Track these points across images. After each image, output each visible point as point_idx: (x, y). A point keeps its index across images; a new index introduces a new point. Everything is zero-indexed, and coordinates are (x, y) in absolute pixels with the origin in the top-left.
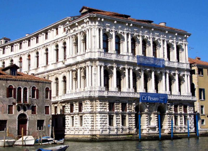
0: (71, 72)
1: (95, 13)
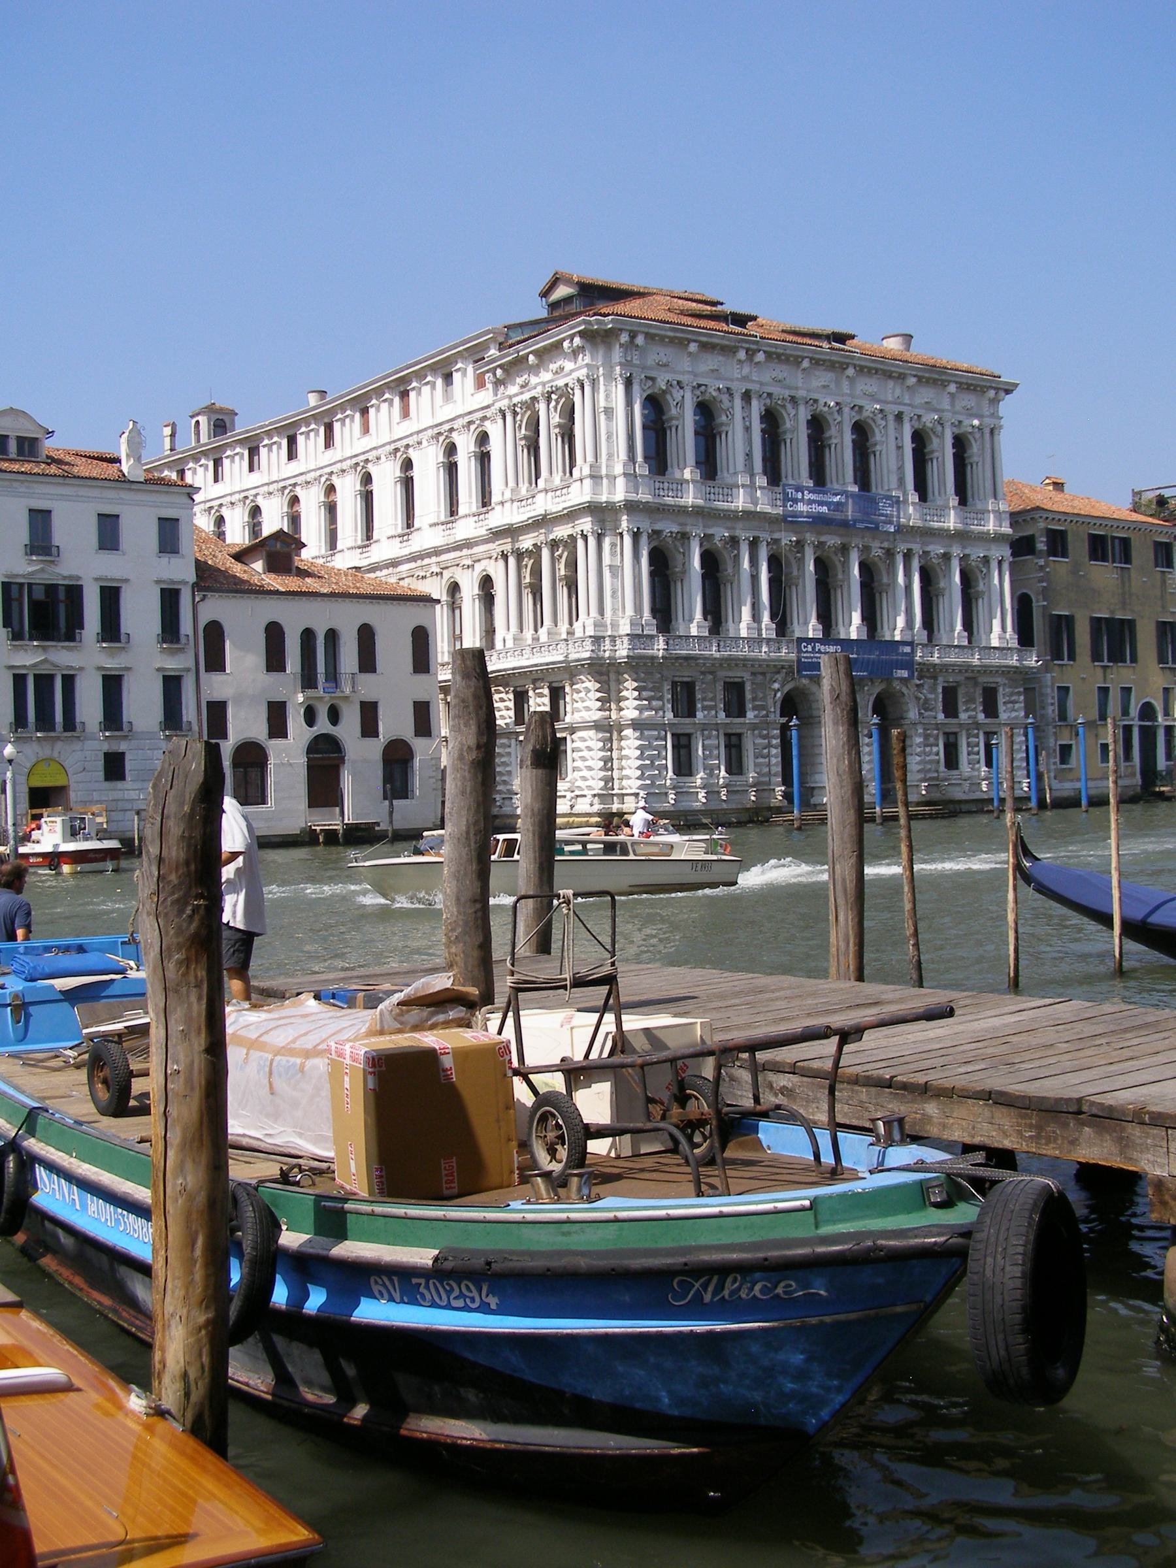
0: (512, 561)
1: (608, 315)
